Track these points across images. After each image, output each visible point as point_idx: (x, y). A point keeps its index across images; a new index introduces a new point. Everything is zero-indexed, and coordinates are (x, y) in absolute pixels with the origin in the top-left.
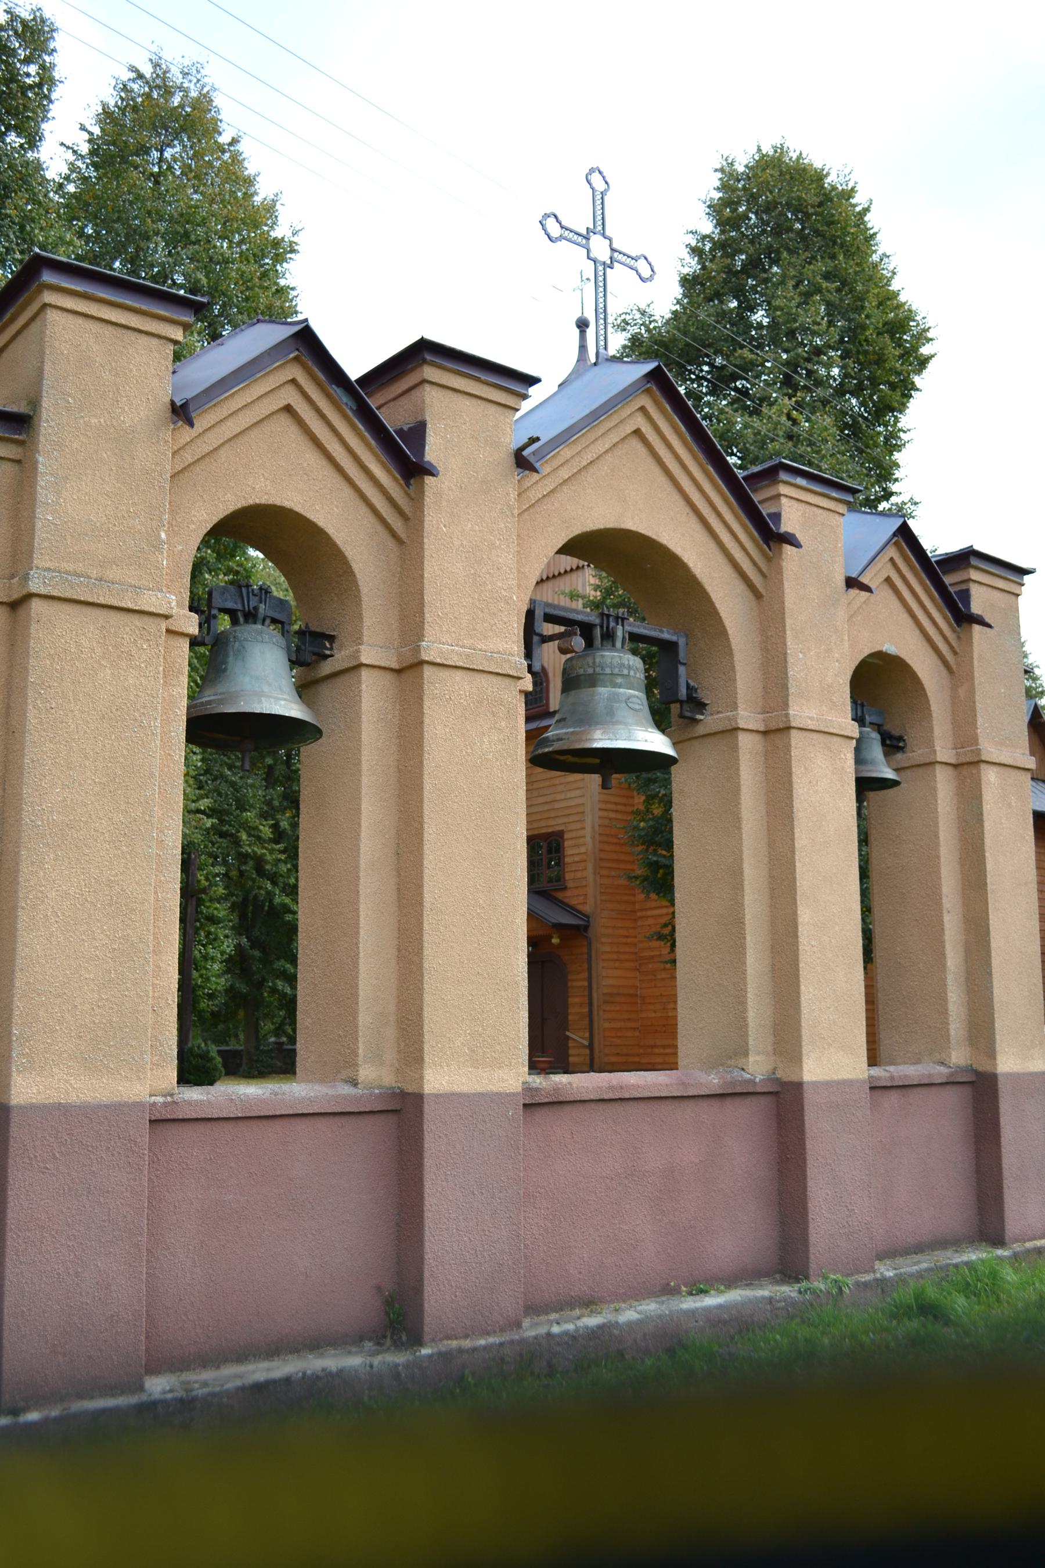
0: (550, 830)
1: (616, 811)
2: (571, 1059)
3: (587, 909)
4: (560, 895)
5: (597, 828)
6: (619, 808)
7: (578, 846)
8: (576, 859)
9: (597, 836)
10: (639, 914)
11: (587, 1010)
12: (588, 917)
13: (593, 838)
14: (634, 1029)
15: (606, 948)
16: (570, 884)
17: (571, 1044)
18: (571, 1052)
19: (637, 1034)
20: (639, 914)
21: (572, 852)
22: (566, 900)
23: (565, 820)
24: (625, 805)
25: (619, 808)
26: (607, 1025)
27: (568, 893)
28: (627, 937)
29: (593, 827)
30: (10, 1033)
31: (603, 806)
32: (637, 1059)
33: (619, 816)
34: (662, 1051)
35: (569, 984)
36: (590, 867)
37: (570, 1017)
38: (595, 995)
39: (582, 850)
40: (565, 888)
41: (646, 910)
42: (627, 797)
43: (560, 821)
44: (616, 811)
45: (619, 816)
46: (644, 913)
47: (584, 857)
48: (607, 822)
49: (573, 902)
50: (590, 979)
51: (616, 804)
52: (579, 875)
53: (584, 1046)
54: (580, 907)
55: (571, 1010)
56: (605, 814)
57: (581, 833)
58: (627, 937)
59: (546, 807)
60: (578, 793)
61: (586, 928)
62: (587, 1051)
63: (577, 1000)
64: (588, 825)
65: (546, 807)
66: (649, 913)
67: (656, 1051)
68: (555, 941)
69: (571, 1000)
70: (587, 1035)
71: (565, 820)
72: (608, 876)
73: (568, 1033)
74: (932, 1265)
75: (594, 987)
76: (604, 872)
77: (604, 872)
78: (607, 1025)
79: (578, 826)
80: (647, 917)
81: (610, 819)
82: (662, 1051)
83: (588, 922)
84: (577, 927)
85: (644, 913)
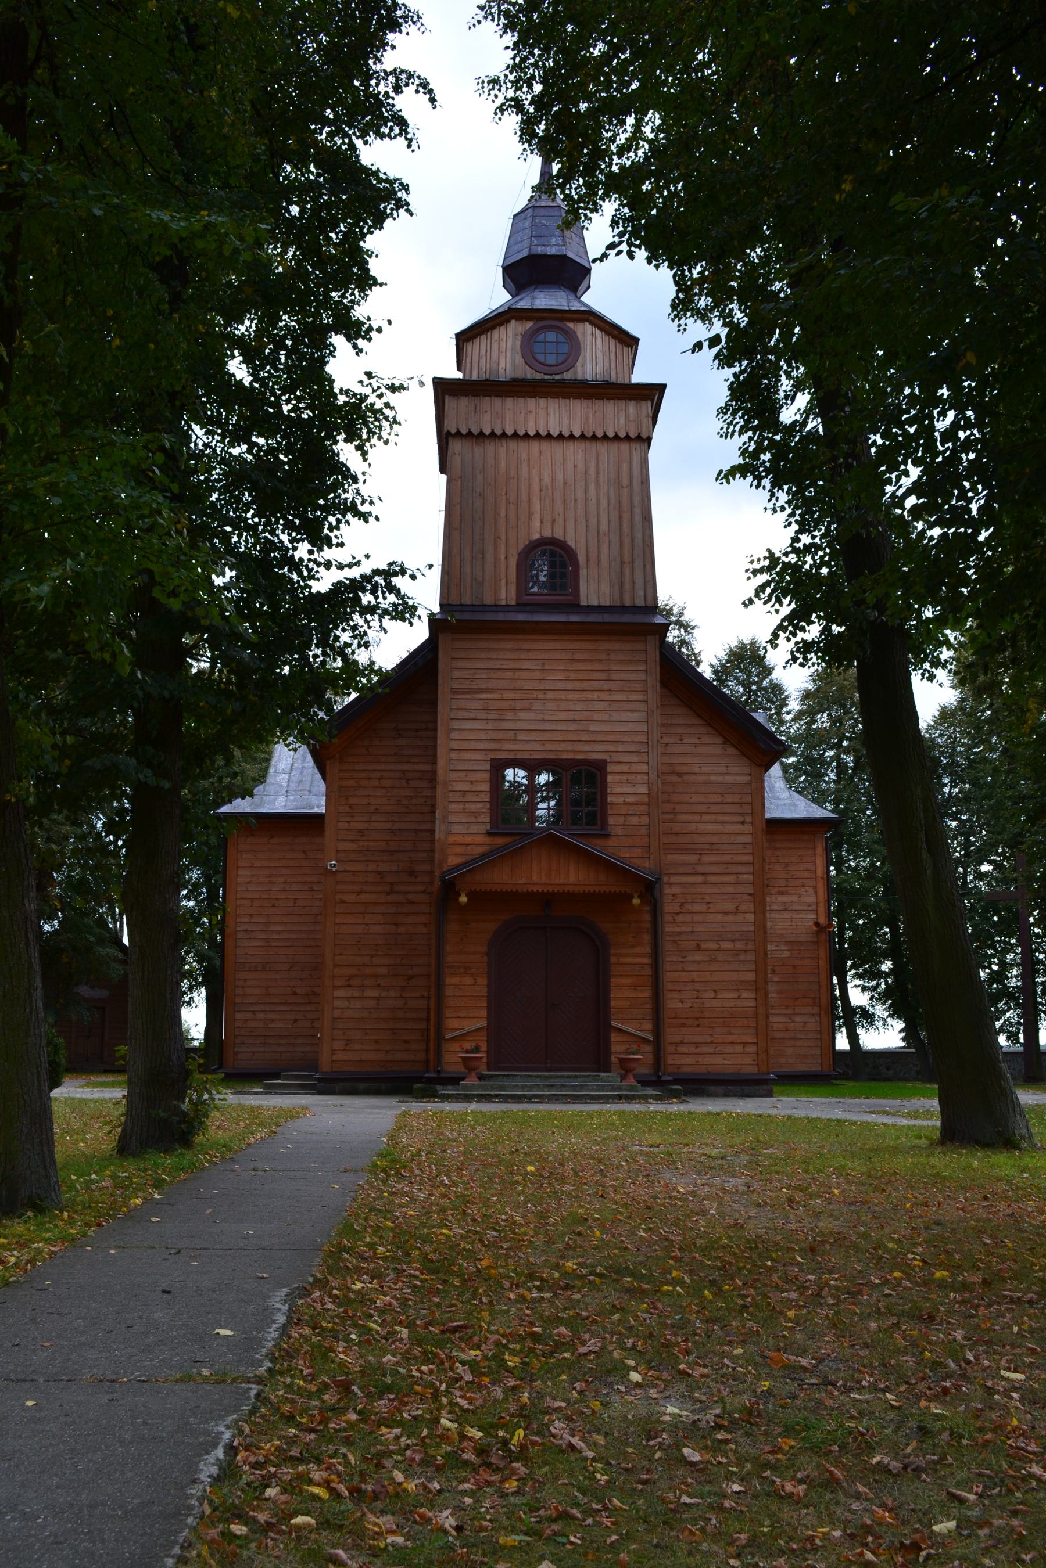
23: (611, 748)
27: (612, 842)
34: (692, 1049)
40: (607, 836)
71: (611, 748)
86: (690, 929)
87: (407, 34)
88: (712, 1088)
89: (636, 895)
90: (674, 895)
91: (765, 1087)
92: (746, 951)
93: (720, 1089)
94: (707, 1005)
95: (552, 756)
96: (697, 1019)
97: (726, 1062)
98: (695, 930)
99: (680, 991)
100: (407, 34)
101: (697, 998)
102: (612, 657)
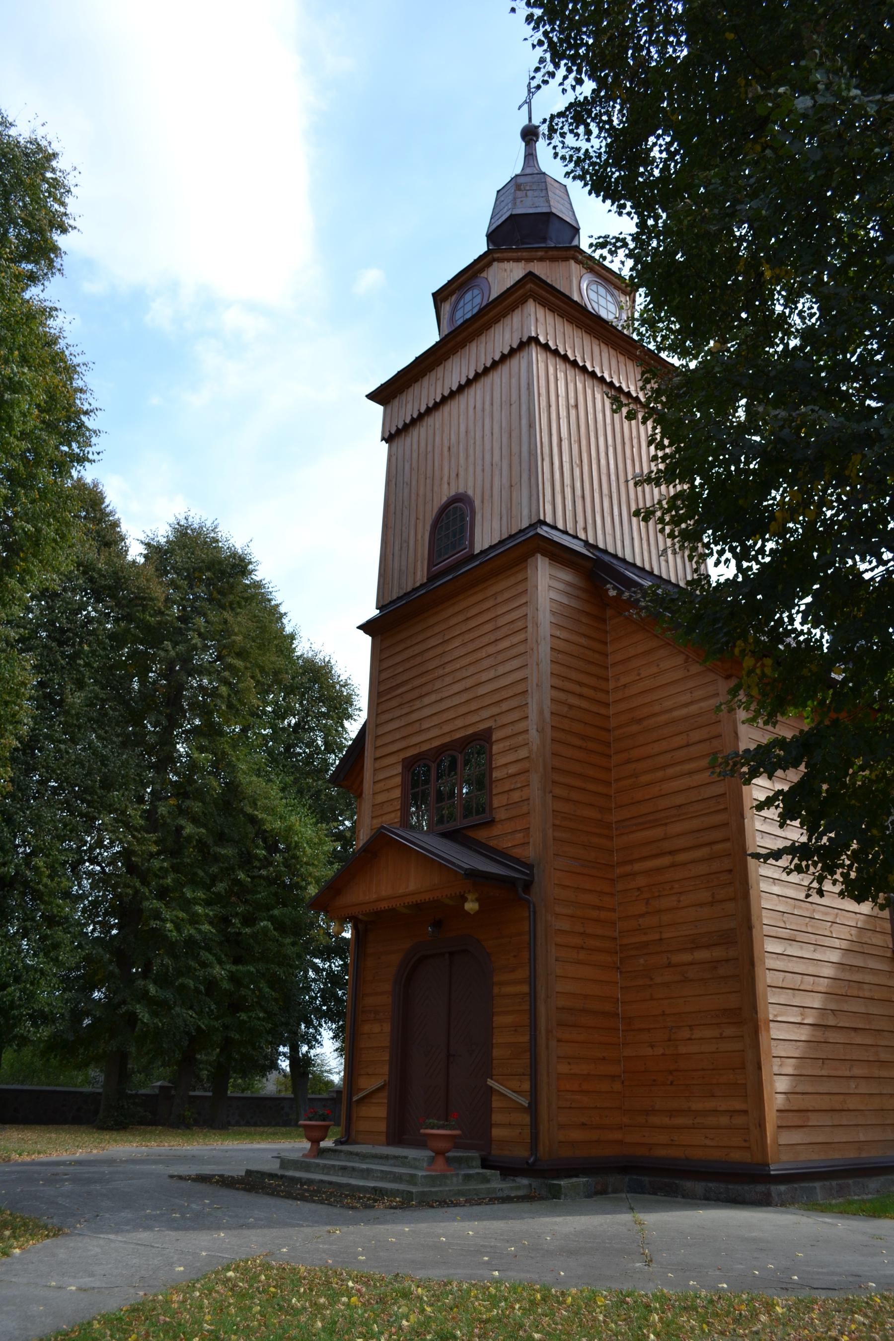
0: (470, 731)
1: (581, 696)
2: (496, 1132)
3: (529, 853)
4: (482, 835)
5: (547, 714)
6: (585, 691)
7: (515, 749)
8: (512, 770)
9: (548, 730)
10: (618, 871)
11: (526, 1038)
12: (530, 867)
13: (541, 731)
14: (613, 1077)
15: (565, 925)
16: (501, 815)
17: (496, 1103)
18: (496, 1118)
19: (617, 1087)
20: (618, 871)
21: (503, 760)
22: (492, 843)
23: (495, 710)
24: (595, 688)
25: (585, 691)
26: (563, 1068)
27: (496, 830)
28: (599, 908)
29: (541, 712)
30: (475, 1220)
31: (558, 683)
32: (617, 1136)
33: (584, 704)
34: (666, 1120)
35: (496, 990)
36: (535, 779)
37: (496, 1053)
38: (542, 1009)
39: (523, 753)
40: (491, 823)
41: (631, 862)
42: (599, 677)
43: (485, 714)
44: (581, 696)
45: (584, 704)
46: (628, 868)
47: (526, 765)
48: (565, 710)
49: (505, 844)
50: (532, 981)
51: (580, 684)
52: (516, 796)
53: (519, 1108)
54: (517, 852)
55: (498, 1039)
56: (562, 696)
57: (521, 726)
58: (599, 908)
59: (465, 697)
60: (516, 663)
61: (528, 886)
62: (527, 1119)
63: (508, 1019)
64: (533, 712)
65: (465, 697)
66: (637, 867)
67: (655, 1120)
68: (471, 906)
69: (498, 1020)
70: (526, 1086)
71: (495, 710)
72: (567, 800)
73: (490, 1082)
74: (572, 1229)
75: (542, 994)
76: (558, 791)
77: (558, 791)
78: (563, 1068)
79: (515, 716)
80: (634, 875)
81: (571, 706)
82: (666, 1120)
83: (532, 875)
84: (509, 883)
85: (628, 868)
86: (657, 937)
87: (610, 211)
88: (689, 1184)
89: (470, 897)
90: (639, 889)
91: (761, 1188)
92: (727, 961)
93: (699, 1187)
94: (683, 1050)
95: (447, 739)
96: (671, 1072)
97: (708, 1142)
98: (665, 936)
99: (649, 1030)
100: (610, 211)
101: (669, 1040)
102: (500, 599)
